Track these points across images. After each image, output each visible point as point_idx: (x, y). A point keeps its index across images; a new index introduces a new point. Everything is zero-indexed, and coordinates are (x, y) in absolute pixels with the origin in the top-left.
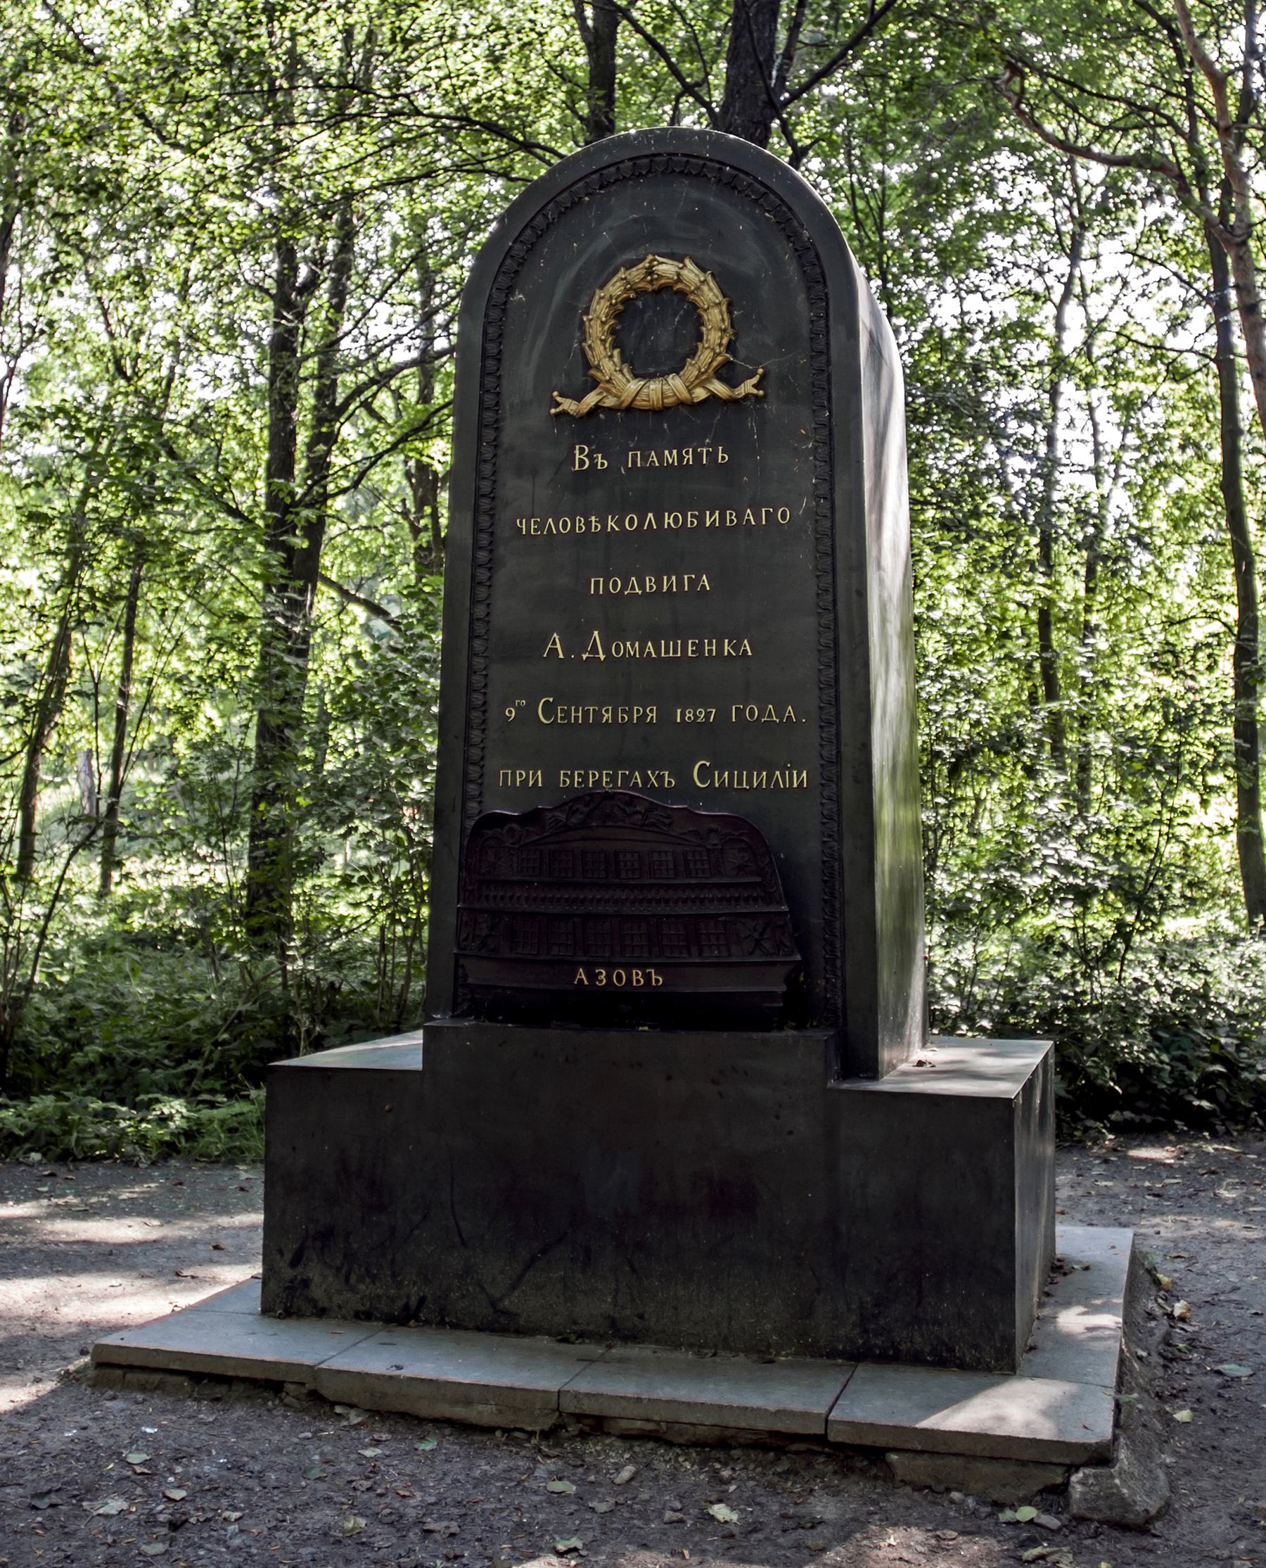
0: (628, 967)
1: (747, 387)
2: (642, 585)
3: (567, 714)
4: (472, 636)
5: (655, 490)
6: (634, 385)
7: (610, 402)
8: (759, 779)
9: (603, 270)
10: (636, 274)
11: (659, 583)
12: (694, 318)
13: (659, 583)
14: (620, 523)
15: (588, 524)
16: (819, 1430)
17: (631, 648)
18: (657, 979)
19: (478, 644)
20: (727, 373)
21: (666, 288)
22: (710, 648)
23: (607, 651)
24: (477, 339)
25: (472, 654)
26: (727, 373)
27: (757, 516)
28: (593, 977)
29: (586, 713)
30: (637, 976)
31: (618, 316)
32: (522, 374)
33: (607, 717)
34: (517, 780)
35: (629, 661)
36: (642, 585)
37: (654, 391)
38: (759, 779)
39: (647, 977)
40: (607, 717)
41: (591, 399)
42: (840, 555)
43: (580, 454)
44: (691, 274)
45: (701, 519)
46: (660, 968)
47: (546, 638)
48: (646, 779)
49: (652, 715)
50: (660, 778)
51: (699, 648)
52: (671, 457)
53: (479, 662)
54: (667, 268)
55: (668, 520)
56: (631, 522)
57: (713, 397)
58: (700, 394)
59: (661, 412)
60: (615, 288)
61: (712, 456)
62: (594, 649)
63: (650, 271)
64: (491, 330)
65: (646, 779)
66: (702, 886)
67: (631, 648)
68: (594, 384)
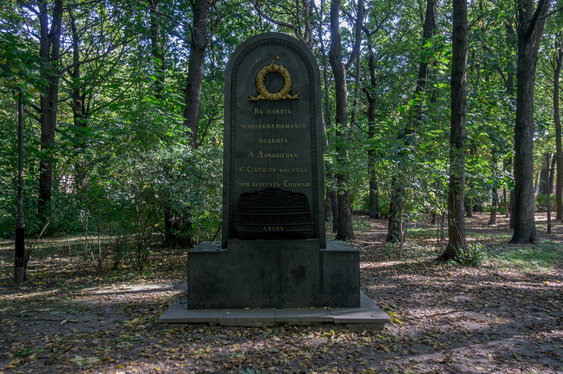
0: (276, 226)
1: (295, 96)
2: (271, 141)
3: (254, 170)
4: (231, 152)
5: (275, 119)
6: (269, 95)
7: (263, 98)
8: (299, 185)
9: (260, 66)
10: (269, 68)
11: (275, 141)
12: (283, 79)
13: (275, 141)
14: (266, 127)
15: (258, 126)
16: (332, 321)
17: (269, 155)
18: (282, 229)
19: (232, 153)
20: (290, 93)
21: (277, 72)
22: (287, 156)
23: (263, 156)
24: (316, 85)
25: (231, 156)
26: (290, 93)
27: (298, 126)
28: (267, 229)
29: (259, 170)
30: (278, 228)
31: (264, 77)
32: (241, 90)
33: (264, 171)
34: (244, 185)
35: (268, 158)
36: (271, 141)
37: (275, 96)
38: (299, 185)
39: (280, 228)
40: (264, 171)
41: (259, 97)
42: (317, 135)
43: (256, 110)
44: (282, 68)
45: (285, 126)
46: (283, 226)
47: (249, 153)
48: (273, 185)
49: (274, 171)
50: (276, 185)
51: (285, 155)
52: (278, 112)
53: (233, 158)
54: (276, 67)
55: (277, 126)
56: (269, 126)
57: (288, 98)
58: (285, 98)
59: (274, 101)
60: (264, 71)
61: (287, 112)
62: (261, 155)
63: (273, 67)
64: (233, 79)
65: (273, 185)
66: (293, 209)
67: (269, 155)
68: (259, 94)
